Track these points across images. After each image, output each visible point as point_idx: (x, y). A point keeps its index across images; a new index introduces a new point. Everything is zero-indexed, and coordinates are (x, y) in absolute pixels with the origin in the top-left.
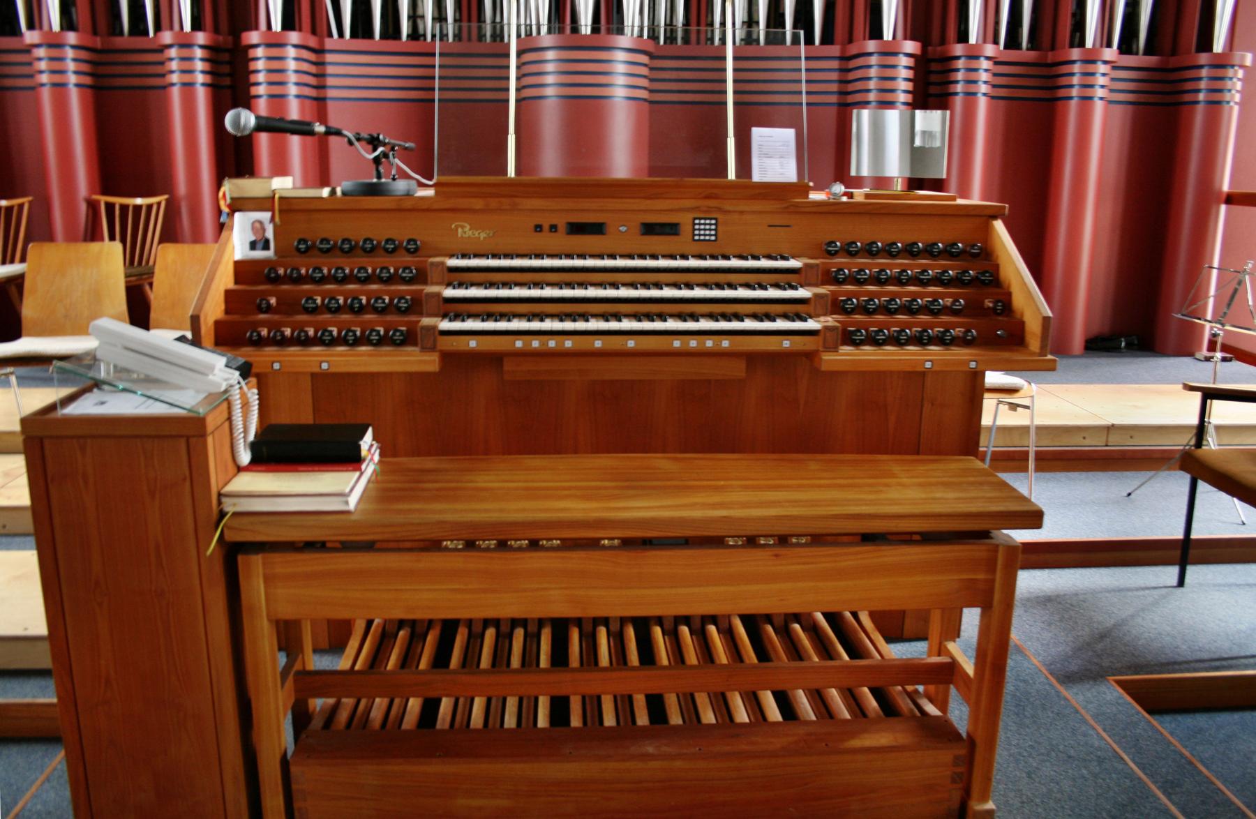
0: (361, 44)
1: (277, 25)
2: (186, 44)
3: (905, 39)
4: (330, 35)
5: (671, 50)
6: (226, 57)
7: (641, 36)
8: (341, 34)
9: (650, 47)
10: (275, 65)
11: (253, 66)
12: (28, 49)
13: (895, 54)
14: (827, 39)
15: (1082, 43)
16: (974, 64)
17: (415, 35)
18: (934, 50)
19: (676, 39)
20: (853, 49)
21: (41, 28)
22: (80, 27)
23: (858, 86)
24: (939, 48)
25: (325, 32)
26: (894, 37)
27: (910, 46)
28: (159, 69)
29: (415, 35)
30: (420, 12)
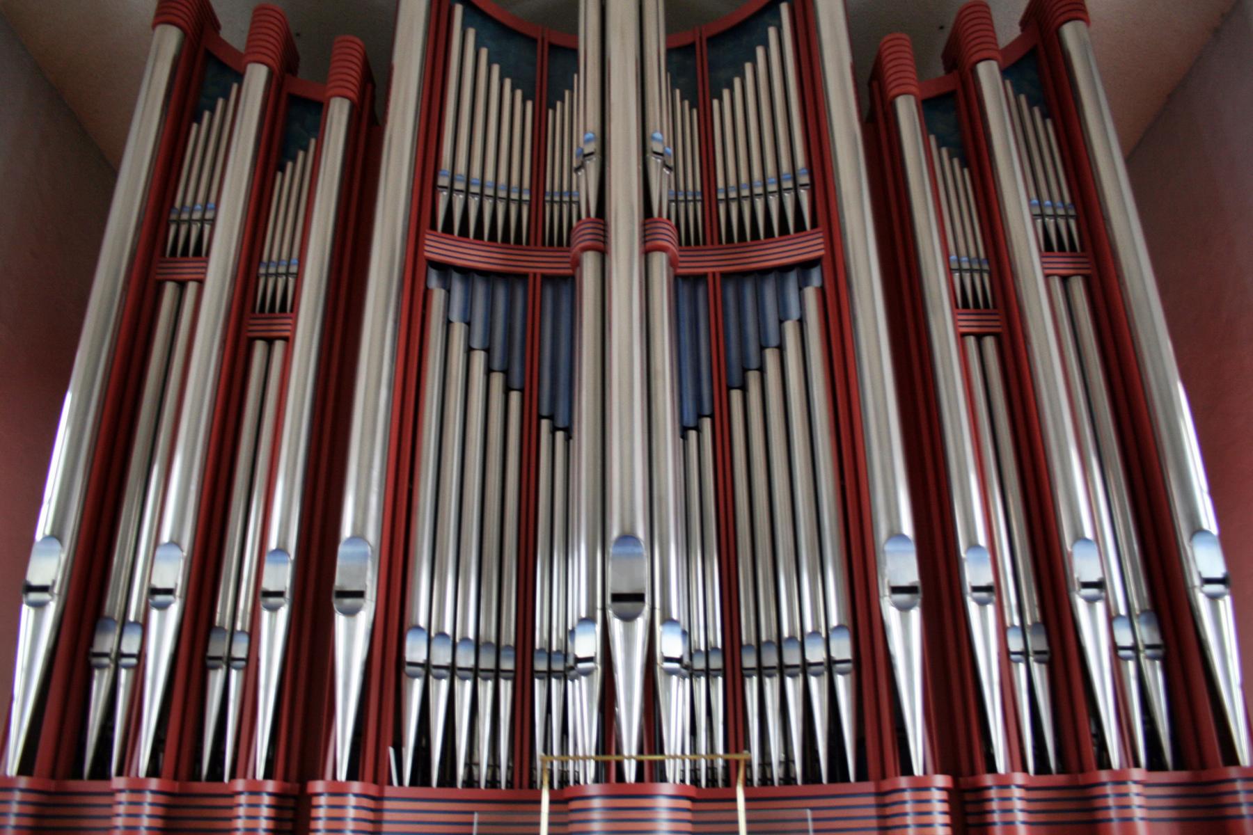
0: (419, 791)
1: (342, 775)
2: (255, 792)
3: (936, 772)
4: (390, 783)
5: (713, 793)
6: (291, 803)
7: (683, 781)
8: (401, 782)
9: (693, 792)
10: (336, 813)
11: (315, 813)
12: (112, 793)
13: (927, 789)
14: (862, 775)
15: (1108, 766)
16: (1006, 793)
17: (470, 782)
18: (965, 781)
19: (716, 781)
20: (887, 785)
21: (128, 775)
22: (164, 774)
23: (895, 809)
24: (970, 779)
25: (386, 778)
26: (925, 772)
27: (941, 780)
28: (226, 813)
29: (470, 782)
30: (476, 760)
